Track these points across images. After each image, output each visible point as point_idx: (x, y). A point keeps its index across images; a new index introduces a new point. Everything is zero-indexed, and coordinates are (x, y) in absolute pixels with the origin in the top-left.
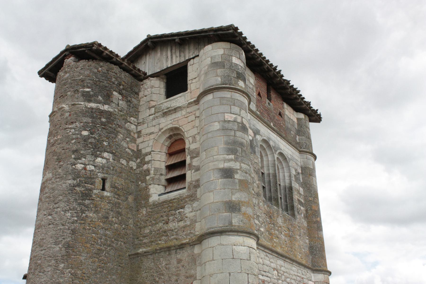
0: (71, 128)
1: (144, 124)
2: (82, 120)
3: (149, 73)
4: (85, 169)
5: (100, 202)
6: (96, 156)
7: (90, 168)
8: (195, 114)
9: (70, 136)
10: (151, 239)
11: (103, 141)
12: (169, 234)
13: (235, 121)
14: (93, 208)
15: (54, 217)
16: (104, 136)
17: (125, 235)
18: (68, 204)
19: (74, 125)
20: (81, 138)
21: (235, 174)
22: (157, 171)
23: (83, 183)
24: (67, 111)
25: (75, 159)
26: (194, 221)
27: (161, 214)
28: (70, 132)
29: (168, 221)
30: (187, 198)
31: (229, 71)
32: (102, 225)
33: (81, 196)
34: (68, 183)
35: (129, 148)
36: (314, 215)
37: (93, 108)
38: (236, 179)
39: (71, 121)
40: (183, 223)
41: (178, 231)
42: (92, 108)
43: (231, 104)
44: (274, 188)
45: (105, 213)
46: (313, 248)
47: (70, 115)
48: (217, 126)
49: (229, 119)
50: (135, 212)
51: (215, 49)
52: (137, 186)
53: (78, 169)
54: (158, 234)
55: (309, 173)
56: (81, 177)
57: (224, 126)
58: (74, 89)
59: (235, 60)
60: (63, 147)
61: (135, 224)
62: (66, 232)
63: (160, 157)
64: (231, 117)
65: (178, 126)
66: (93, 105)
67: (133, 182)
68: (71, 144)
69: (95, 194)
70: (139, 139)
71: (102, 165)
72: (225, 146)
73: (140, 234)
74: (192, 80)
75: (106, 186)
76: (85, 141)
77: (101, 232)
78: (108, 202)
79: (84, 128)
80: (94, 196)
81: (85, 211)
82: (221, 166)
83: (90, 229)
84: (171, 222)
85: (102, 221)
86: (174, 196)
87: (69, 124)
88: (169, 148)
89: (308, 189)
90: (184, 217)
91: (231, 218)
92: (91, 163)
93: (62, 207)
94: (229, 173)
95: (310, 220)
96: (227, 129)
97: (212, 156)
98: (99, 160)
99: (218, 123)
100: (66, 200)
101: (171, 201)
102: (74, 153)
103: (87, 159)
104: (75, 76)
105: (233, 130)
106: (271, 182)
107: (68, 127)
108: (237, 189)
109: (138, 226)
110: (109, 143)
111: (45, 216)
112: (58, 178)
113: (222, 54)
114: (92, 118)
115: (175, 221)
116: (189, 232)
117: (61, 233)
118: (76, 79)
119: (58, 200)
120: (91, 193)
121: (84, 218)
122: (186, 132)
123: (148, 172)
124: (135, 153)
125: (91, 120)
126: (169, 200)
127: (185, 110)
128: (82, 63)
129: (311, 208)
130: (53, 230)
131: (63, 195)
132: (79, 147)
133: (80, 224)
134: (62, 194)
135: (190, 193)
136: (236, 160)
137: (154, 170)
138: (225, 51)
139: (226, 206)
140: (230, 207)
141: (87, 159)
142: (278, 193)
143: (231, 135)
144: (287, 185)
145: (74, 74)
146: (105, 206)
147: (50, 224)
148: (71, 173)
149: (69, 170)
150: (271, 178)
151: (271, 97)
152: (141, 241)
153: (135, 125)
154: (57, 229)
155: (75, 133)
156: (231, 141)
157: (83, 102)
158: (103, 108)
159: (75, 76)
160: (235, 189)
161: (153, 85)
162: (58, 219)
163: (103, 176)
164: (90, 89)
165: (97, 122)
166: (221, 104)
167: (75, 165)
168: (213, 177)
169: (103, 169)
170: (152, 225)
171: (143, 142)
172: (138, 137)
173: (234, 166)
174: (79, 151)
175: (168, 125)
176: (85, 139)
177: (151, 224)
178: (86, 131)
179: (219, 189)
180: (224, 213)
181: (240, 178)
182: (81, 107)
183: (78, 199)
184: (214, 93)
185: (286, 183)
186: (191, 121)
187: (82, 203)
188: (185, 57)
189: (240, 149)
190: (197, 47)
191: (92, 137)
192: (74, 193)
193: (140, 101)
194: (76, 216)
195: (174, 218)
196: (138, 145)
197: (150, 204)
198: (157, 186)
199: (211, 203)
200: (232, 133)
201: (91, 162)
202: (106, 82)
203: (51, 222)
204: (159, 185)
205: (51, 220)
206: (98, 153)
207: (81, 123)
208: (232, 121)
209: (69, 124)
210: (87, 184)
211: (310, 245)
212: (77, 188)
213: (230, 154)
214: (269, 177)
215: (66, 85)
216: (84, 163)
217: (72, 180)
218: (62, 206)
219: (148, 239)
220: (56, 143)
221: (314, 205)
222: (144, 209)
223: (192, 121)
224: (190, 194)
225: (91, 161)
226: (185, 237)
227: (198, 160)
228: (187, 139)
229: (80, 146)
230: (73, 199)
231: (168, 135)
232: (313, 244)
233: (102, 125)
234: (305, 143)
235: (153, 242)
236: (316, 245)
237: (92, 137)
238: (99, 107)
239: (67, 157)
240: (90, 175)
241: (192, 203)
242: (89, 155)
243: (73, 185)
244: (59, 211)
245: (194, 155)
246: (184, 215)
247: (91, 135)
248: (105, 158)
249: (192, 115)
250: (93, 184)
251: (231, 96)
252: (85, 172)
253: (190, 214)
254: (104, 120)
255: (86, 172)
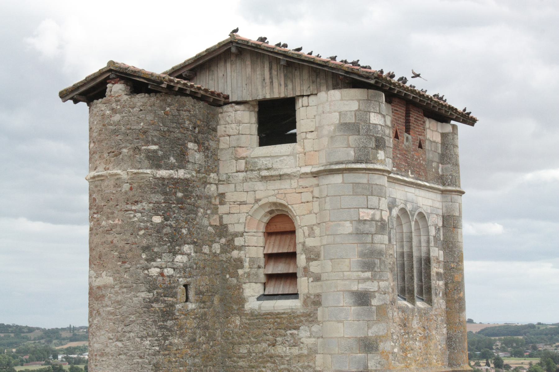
0: (135, 211)
1: (229, 183)
2: (151, 199)
3: (232, 99)
4: (162, 274)
5: (185, 321)
6: (175, 254)
7: (168, 272)
8: (312, 192)
9: (135, 223)
10: (251, 363)
11: (182, 228)
12: (277, 361)
13: (372, 220)
14: (177, 331)
15: (126, 345)
16: (182, 220)
17: (213, 355)
18: (145, 328)
19: (139, 205)
20: (153, 228)
21: (372, 300)
22: (254, 262)
23: (162, 297)
24: (126, 182)
25: (147, 260)
26: (313, 351)
27: (264, 330)
28: (135, 216)
29: (276, 343)
30: (302, 316)
31: (366, 139)
32: (189, 352)
33: (161, 316)
34: (142, 297)
35: (211, 226)
36: (456, 289)
37: (165, 177)
38: (373, 306)
39: (134, 200)
40: (298, 350)
41: (290, 360)
42: (163, 179)
43: (368, 193)
44: (408, 275)
45: (191, 334)
46: (452, 340)
47: (131, 189)
48: (348, 228)
49: (365, 218)
50: (223, 319)
51: (346, 100)
52: (224, 280)
53: (153, 276)
54: (260, 358)
55: (453, 224)
56: (159, 288)
57: (358, 228)
58: (132, 145)
59: (375, 119)
60: (126, 240)
61: (223, 336)
62: (146, 368)
63: (256, 241)
64: (368, 214)
65: (286, 204)
66: (163, 173)
67: (218, 274)
68: (138, 237)
69: (178, 310)
70: (222, 206)
71: (183, 265)
72: (359, 259)
73: (233, 353)
74: (306, 132)
75: (190, 295)
76: (158, 232)
77: (189, 362)
78: (193, 318)
79: (155, 211)
80: (177, 314)
81: (168, 337)
82: (355, 288)
83: (176, 362)
84: (279, 345)
85: (190, 347)
86: (283, 310)
87: (131, 204)
88: (268, 224)
89: (450, 251)
90: (299, 343)
91: (367, 360)
92: (169, 265)
93: (137, 332)
94: (365, 298)
95: (450, 299)
96: (363, 234)
97: (341, 272)
98: (179, 258)
99: (350, 223)
100: (141, 322)
101: (277, 315)
102: (145, 251)
103: (164, 260)
104: (131, 122)
105: (370, 234)
106: (405, 266)
107: (130, 208)
108: (374, 321)
109: (228, 339)
110: (189, 230)
111: (111, 341)
112: (125, 287)
113: (356, 111)
114: (164, 195)
115: (285, 345)
116: (306, 364)
117: (140, 369)
118: (135, 127)
119: (128, 321)
120: (174, 309)
121: (168, 347)
122: (299, 216)
123: (239, 263)
124: (217, 229)
125: (163, 197)
126: (275, 313)
127: (296, 181)
128: (140, 99)
129: (452, 280)
130: (128, 363)
131: (136, 314)
132: (151, 241)
133: (164, 355)
134: (135, 313)
135: (307, 310)
136: (373, 279)
137: (249, 261)
138: (361, 105)
139: (361, 344)
140: (365, 346)
141: (164, 260)
142: (413, 282)
143: (368, 242)
144: (423, 255)
145: (130, 118)
146: (191, 324)
147: (120, 354)
148: (144, 283)
149: (141, 277)
150: (405, 259)
151: (410, 124)
152: (236, 363)
153: (215, 184)
154: (133, 363)
155: (144, 220)
156: (367, 251)
157: (150, 168)
158: (178, 175)
159: (131, 122)
160: (372, 321)
161: (240, 119)
162: (132, 349)
163: (186, 281)
164: (157, 146)
165: (171, 200)
166: (355, 194)
167: (147, 269)
168: (342, 303)
169: (185, 272)
170: (252, 343)
171: (230, 213)
172: (220, 203)
173: (371, 288)
174: (152, 248)
175: (269, 196)
176: (159, 228)
177: (250, 341)
178: (158, 216)
179: (351, 320)
180: (357, 354)
181: (378, 304)
182: (147, 177)
183: (157, 320)
184: (345, 175)
185: (422, 253)
186: (306, 201)
187: (163, 326)
188: (294, 89)
189: (379, 261)
190: (314, 79)
191: (167, 226)
192: (152, 312)
193: (219, 141)
194: (157, 345)
195: (285, 341)
196: (222, 216)
197: (245, 312)
198: (253, 284)
199: (340, 338)
200: (369, 239)
201: (169, 263)
202: (178, 131)
203: (123, 351)
204: (256, 283)
205: (121, 349)
206: (177, 248)
207: (150, 203)
208: (368, 221)
209: (131, 204)
210: (168, 297)
211: (448, 335)
212: (154, 305)
213: (366, 271)
214: (403, 257)
215: (117, 136)
216: (160, 266)
217: (146, 292)
218: (136, 329)
219: (246, 361)
220: (114, 230)
221: (457, 275)
222: (238, 318)
223: (308, 202)
224: (307, 312)
225: (169, 262)
226: (301, 370)
227: (319, 265)
228: (301, 228)
229: (152, 240)
230: (151, 321)
231: (268, 209)
232: (452, 333)
233: (178, 204)
234: (450, 175)
235: (253, 367)
236: (456, 335)
237: (167, 225)
238: (172, 176)
239: (135, 256)
240: (170, 283)
241: (310, 325)
242: (166, 254)
243: (148, 300)
244: (133, 337)
245: (312, 256)
246: (299, 339)
247: (166, 222)
248: (186, 254)
249: (307, 192)
250: (174, 295)
251: (368, 181)
252: (163, 279)
253: (307, 339)
254: (180, 195)
255: (164, 279)
